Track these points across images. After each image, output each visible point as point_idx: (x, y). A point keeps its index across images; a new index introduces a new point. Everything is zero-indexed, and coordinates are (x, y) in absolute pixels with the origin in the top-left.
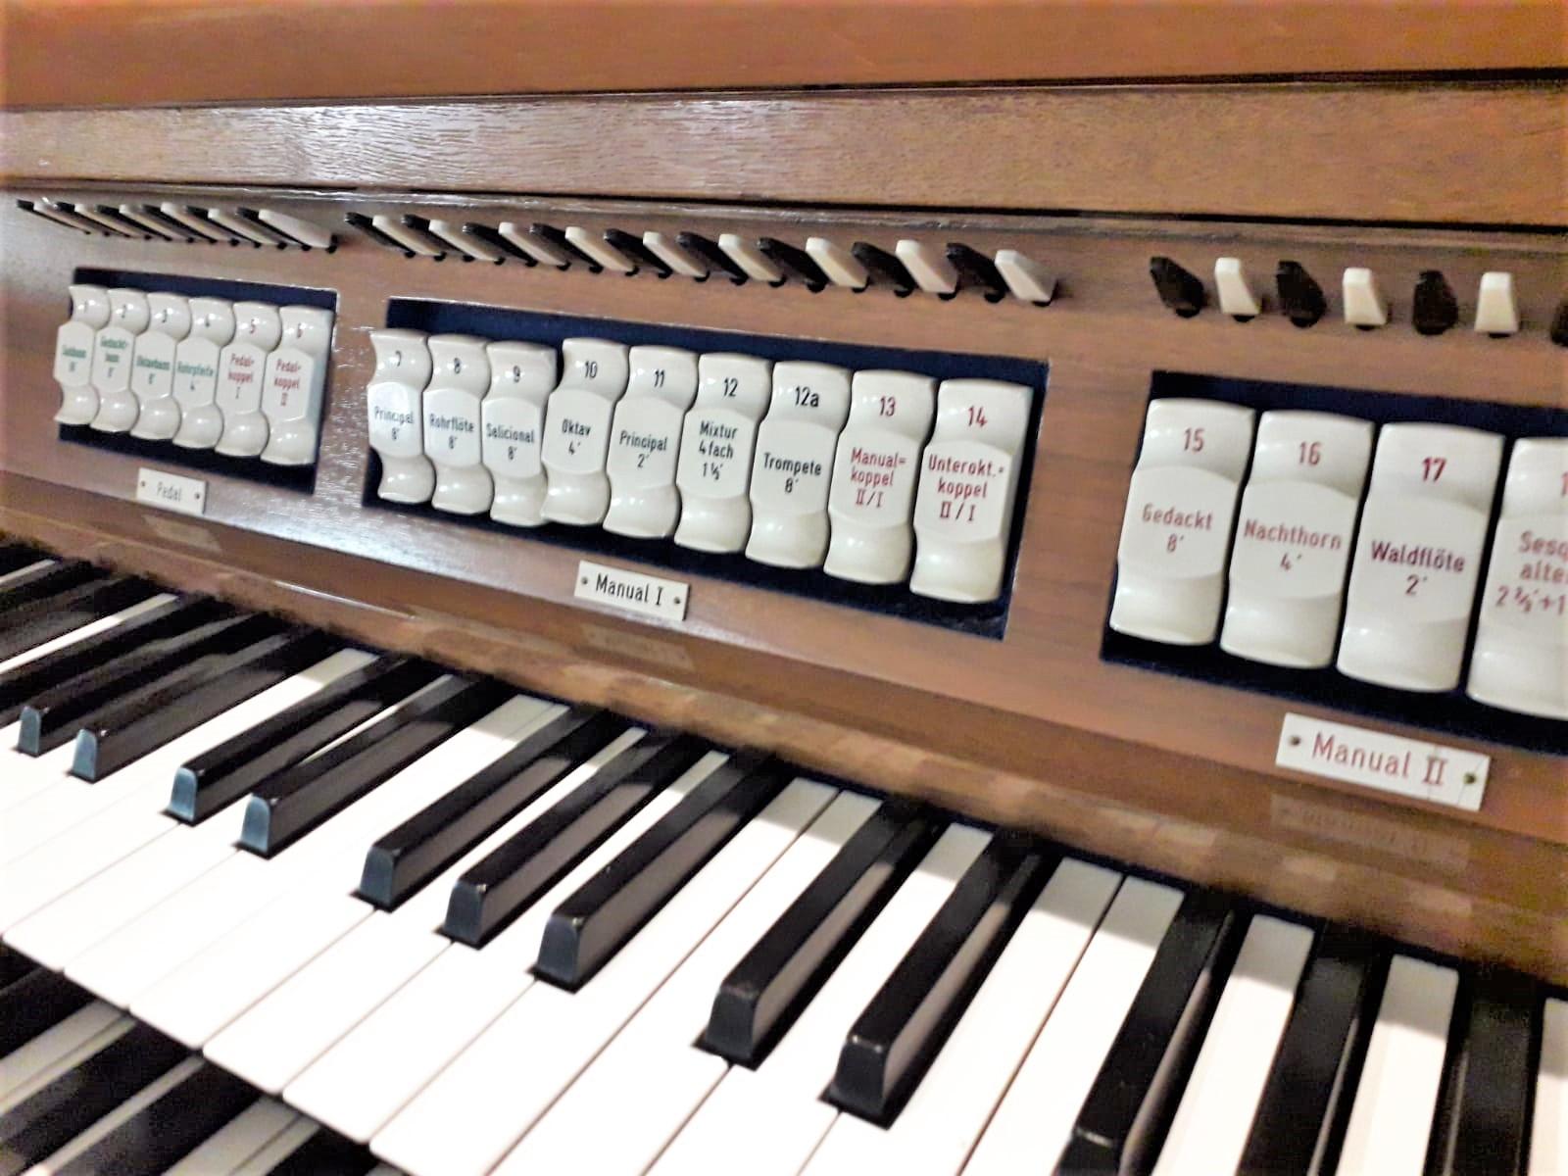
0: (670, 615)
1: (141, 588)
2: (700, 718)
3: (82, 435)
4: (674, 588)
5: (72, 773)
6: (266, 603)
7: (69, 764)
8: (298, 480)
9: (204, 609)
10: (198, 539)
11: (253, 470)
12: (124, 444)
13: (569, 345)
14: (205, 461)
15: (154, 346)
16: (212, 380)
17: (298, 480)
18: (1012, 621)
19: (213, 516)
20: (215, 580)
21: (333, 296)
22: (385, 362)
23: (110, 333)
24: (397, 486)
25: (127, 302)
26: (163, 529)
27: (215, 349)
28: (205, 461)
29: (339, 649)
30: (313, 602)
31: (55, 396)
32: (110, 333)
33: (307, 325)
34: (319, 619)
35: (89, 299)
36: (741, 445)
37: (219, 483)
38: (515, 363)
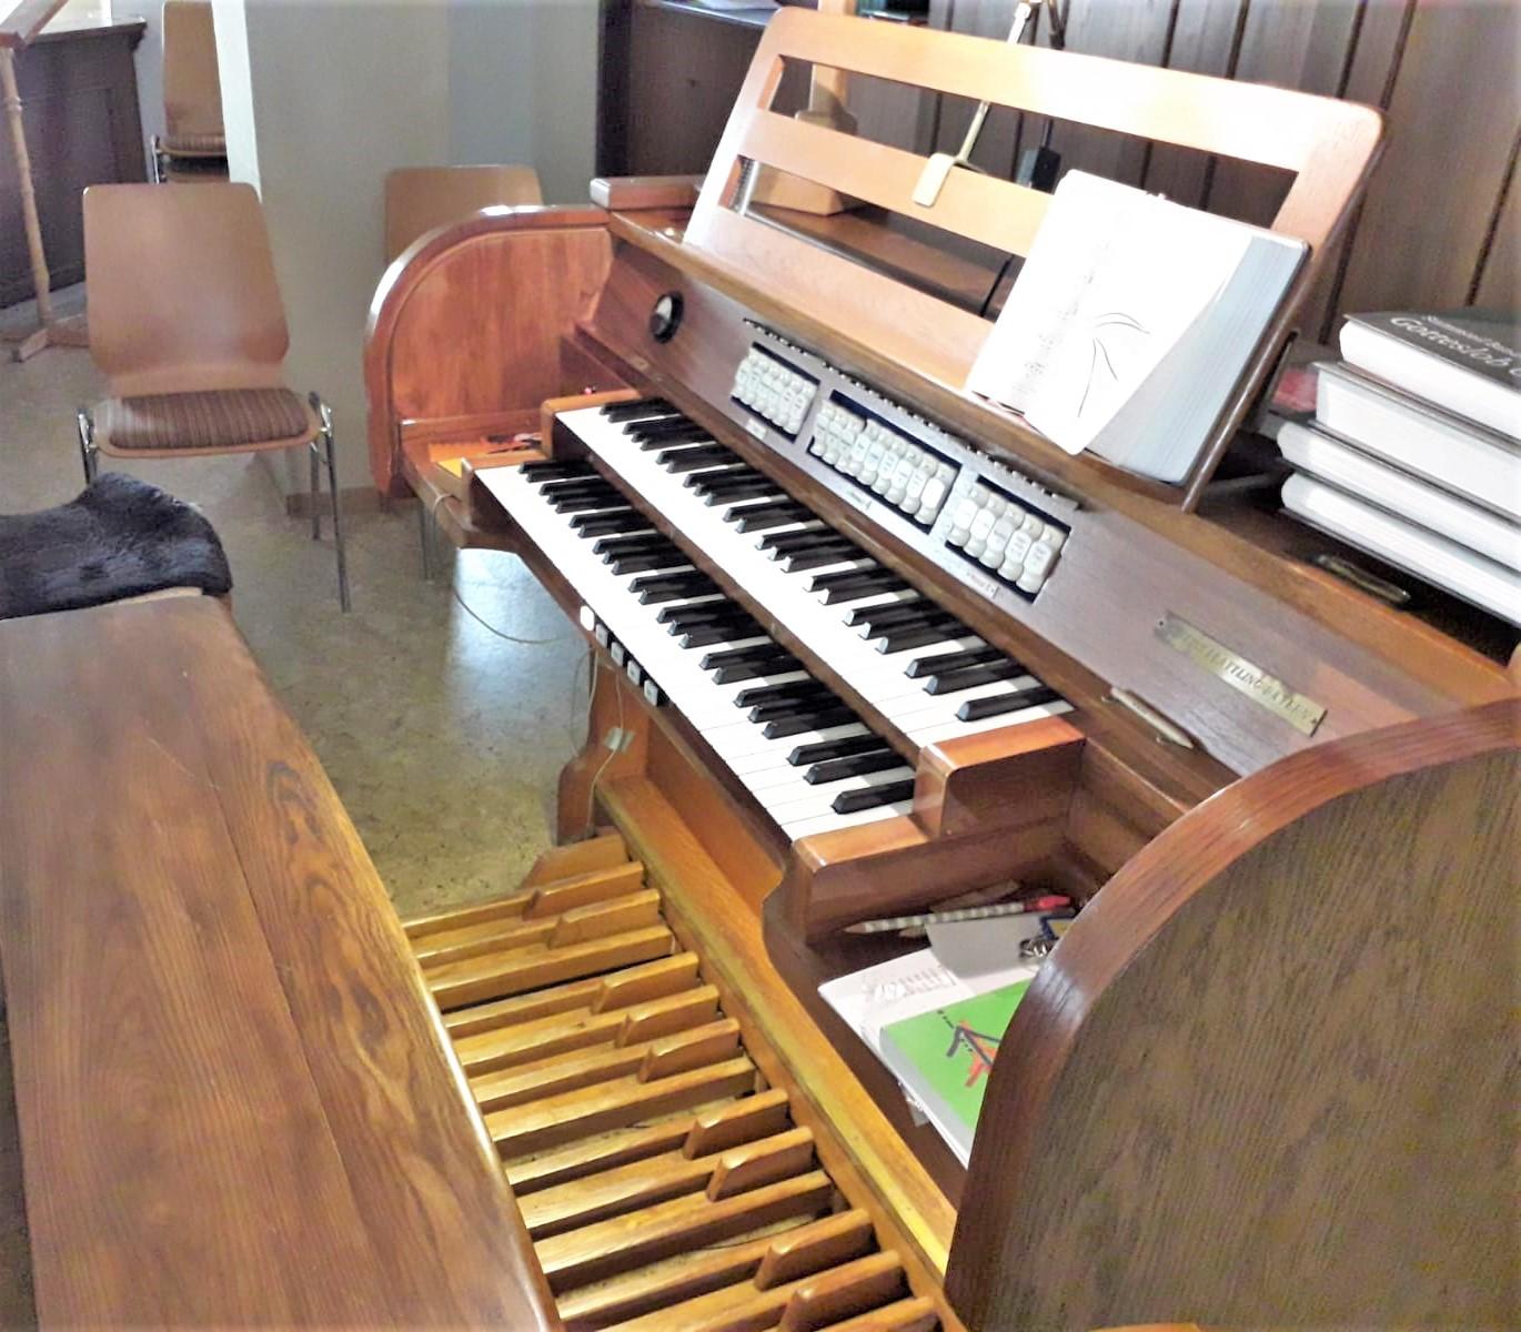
0: (989, 594)
2: (897, 567)
3: (737, 400)
4: (994, 585)
5: (925, 690)
6: (851, 535)
7: (925, 686)
8: (792, 438)
9: (750, 470)
10: (760, 447)
11: (780, 430)
12: (748, 408)
13: (869, 421)
14: (768, 423)
15: (767, 379)
16: (1004, 543)
17: (792, 438)
18: (933, 530)
19: (766, 442)
20: (759, 463)
21: (1070, 528)
22: (824, 411)
23: (757, 370)
24: (816, 449)
25: (764, 360)
26: (751, 441)
27: (993, 519)
28: (768, 423)
29: (971, 635)
31: (731, 382)
32: (757, 370)
33: (809, 388)
34: (866, 546)
35: (754, 354)
37: (771, 431)
38: (853, 421)
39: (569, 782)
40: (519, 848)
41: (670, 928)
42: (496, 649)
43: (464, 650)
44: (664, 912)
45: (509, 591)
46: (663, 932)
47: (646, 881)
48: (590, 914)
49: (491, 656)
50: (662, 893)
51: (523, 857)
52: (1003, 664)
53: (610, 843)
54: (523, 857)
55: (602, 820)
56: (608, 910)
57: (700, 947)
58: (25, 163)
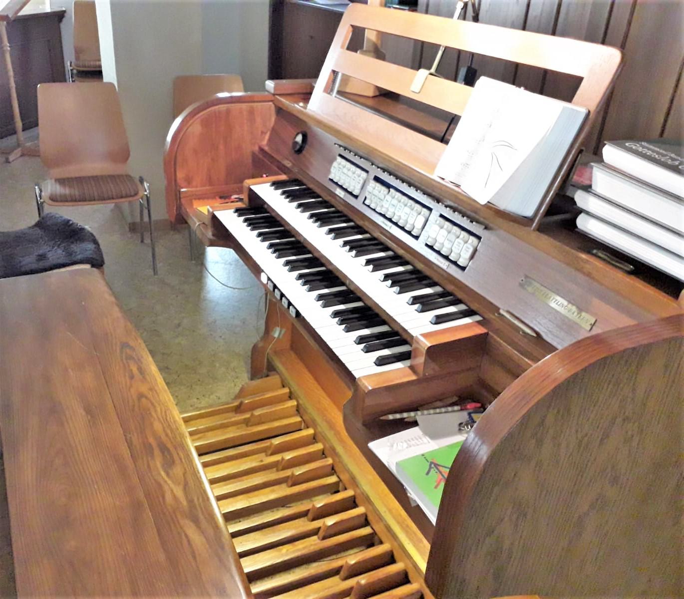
0: (445, 267)
1: (333, 206)
3: (331, 180)
4: (447, 263)
5: (416, 310)
6: (383, 241)
7: (416, 308)
8: (356, 197)
9: (337, 212)
10: (342, 201)
11: (351, 193)
12: (336, 184)
13: (391, 190)
14: (346, 190)
15: (345, 171)
16: (452, 244)
17: (356, 197)
18: (420, 238)
19: (344, 199)
20: (341, 208)
21: (481, 238)
22: (370, 185)
23: (340, 166)
24: (367, 202)
25: (344, 162)
26: (338, 198)
27: (447, 233)
28: (346, 190)
29: (437, 285)
30: (351, 215)
31: (329, 172)
32: (340, 166)
33: (364, 174)
34: (389, 246)
35: (339, 159)
36: (455, 245)
37: (347, 194)
38: (384, 189)
39: (256, 351)
40: (234, 381)
41: (301, 417)
42: (223, 292)
43: (209, 292)
44: (298, 410)
45: (229, 266)
46: (298, 419)
47: (291, 396)
48: (265, 411)
49: (221, 295)
50: (298, 401)
51: (235, 385)
52: (451, 299)
53: (274, 379)
54: (235, 385)
55: (271, 369)
56: (274, 409)
57: (315, 426)
58: (11, 73)
